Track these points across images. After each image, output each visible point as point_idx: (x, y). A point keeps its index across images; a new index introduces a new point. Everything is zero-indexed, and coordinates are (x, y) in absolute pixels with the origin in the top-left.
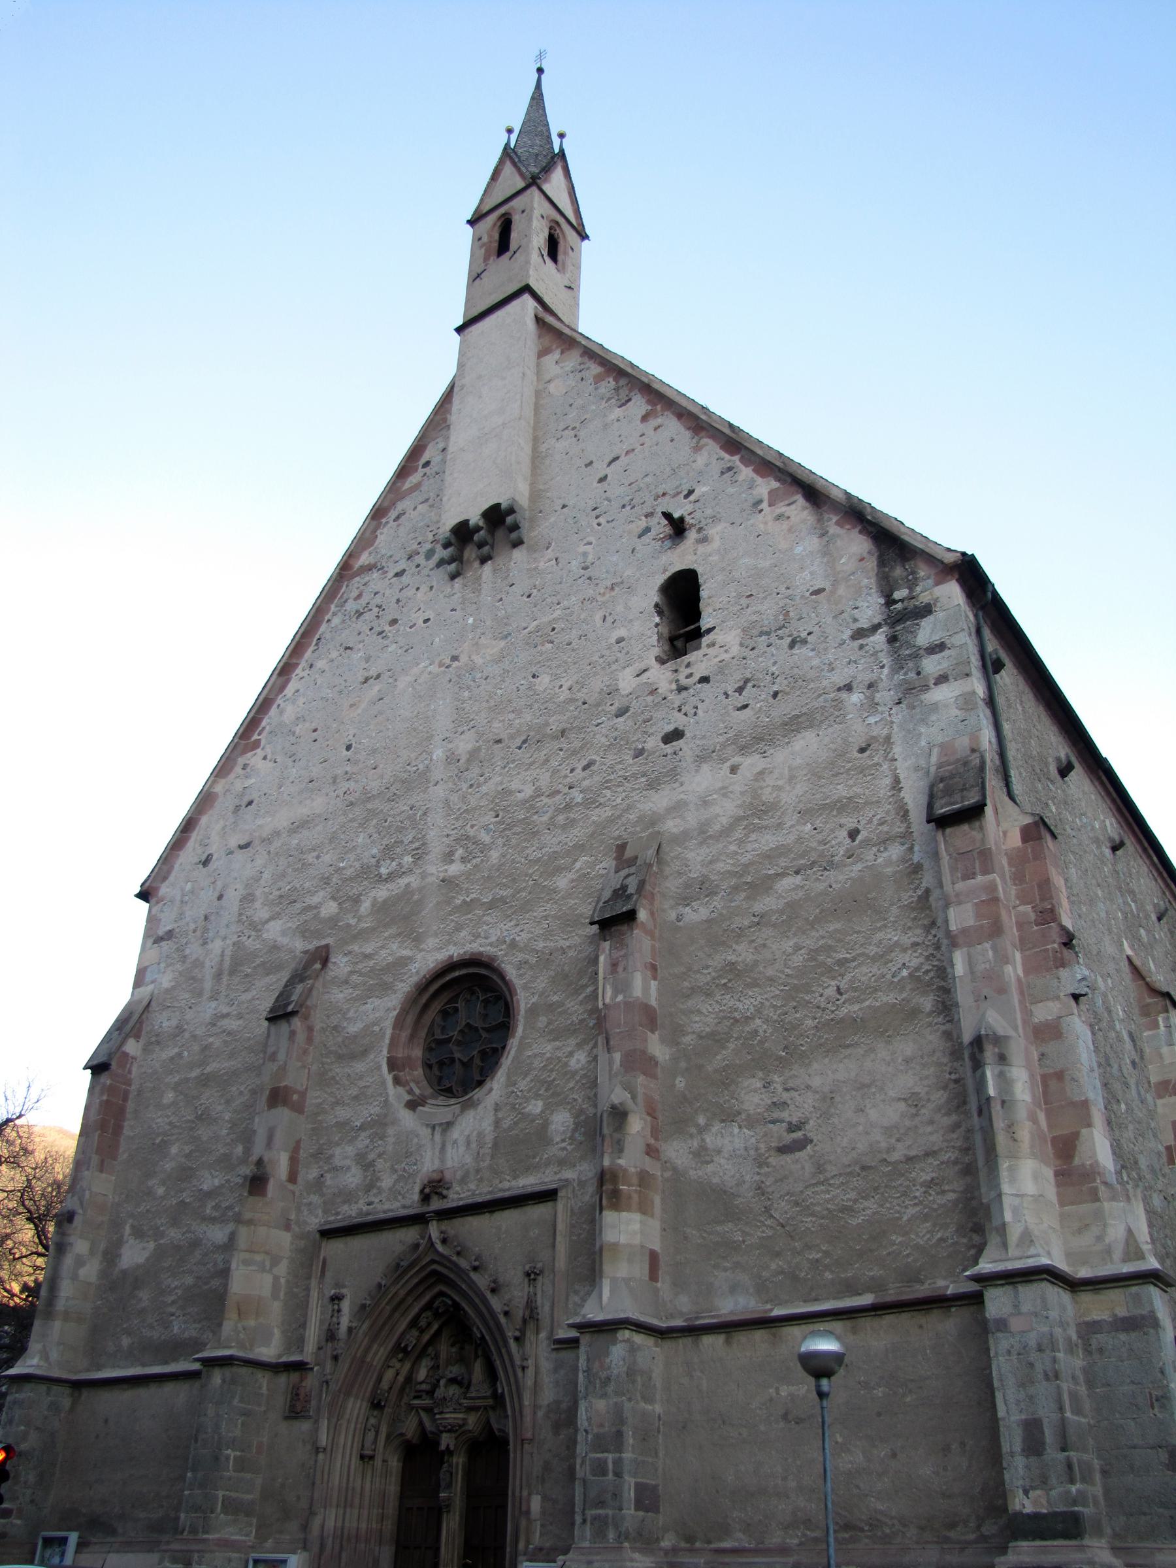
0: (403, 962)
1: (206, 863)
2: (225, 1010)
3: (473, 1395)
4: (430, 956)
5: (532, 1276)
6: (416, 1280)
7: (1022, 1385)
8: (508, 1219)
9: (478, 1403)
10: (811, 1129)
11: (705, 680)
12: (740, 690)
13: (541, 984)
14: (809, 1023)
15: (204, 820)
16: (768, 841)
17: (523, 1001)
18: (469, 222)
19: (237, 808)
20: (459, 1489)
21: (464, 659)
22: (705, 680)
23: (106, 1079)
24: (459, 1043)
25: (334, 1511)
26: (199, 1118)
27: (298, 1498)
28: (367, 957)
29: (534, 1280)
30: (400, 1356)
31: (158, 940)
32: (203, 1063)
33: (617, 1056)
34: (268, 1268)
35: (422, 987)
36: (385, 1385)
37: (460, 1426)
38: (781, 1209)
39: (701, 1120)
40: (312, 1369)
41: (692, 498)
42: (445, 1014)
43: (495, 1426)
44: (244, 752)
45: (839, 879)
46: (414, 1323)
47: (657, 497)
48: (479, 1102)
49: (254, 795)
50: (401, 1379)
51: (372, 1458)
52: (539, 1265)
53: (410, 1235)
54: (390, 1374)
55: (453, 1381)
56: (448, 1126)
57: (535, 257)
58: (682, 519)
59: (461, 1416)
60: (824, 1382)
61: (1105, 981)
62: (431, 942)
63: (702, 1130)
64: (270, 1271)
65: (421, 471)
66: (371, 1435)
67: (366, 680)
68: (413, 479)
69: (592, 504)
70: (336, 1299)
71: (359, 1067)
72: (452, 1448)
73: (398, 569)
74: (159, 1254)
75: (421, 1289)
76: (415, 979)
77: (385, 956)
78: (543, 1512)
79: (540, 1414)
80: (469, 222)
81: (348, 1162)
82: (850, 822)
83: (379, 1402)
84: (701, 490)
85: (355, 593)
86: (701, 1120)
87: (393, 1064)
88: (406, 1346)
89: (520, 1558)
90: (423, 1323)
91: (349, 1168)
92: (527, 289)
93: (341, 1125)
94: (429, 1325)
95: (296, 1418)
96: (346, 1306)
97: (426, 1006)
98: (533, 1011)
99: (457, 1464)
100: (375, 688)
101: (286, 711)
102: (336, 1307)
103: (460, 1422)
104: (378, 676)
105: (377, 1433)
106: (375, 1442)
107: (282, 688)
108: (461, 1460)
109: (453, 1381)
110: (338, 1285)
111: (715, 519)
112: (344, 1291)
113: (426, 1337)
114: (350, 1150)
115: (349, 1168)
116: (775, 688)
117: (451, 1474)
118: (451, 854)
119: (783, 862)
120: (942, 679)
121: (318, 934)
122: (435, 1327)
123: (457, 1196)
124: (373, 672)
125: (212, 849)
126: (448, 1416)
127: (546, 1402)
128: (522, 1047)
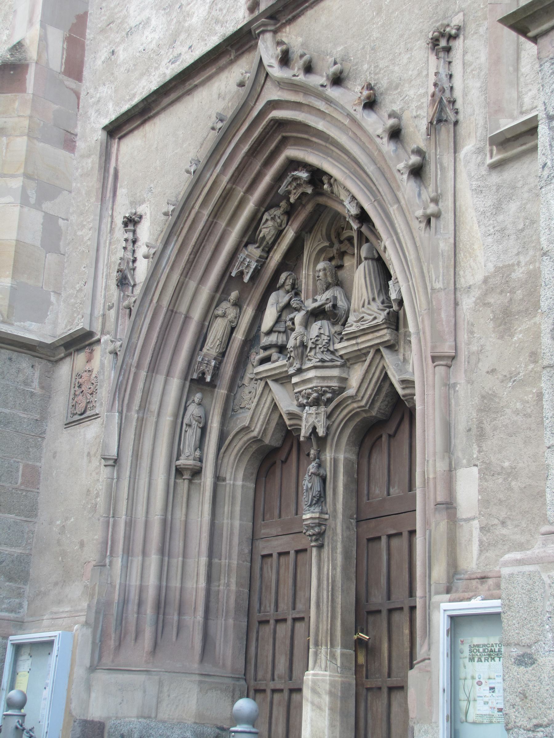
3: (353, 329)
5: (443, 43)
6: (245, 148)
9: (365, 341)
25: (324, 647)
27: (82, 544)
29: (448, 50)
30: (234, 295)
34: (32, 201)
36: (212, 347)
37: (337, 392)
40: (99, 341)
46: (250, 234)
50: (239, 336)
51: (197, 473)
52: (456, 20)
54: (218, 328)
55: (317, 314)
59: (335, 372)
64: (38, 206)
66: (191, 437)
70: (132, 222)
72: (321, 432)
75: (257, 165)
78: (485, 502)
79: (467, 303)
81: (146, 13)
89: (436, 598)
90: (267, 230)
91: (148, 21)
94: (279, 234)
95: (78, 422)
96: (146, 232)
99: (335, 461)
102: (130, 236)
103: (335, 384)
105: (204, 430)
106: (201, 444)
108: (341, 457)
109: (317, 314)
110: (134, 203)
112: (140, 210)
113: (276, 257)
115: (148, 21)
117: (324, 480)
122: (290, 235)
127: (479, 277)
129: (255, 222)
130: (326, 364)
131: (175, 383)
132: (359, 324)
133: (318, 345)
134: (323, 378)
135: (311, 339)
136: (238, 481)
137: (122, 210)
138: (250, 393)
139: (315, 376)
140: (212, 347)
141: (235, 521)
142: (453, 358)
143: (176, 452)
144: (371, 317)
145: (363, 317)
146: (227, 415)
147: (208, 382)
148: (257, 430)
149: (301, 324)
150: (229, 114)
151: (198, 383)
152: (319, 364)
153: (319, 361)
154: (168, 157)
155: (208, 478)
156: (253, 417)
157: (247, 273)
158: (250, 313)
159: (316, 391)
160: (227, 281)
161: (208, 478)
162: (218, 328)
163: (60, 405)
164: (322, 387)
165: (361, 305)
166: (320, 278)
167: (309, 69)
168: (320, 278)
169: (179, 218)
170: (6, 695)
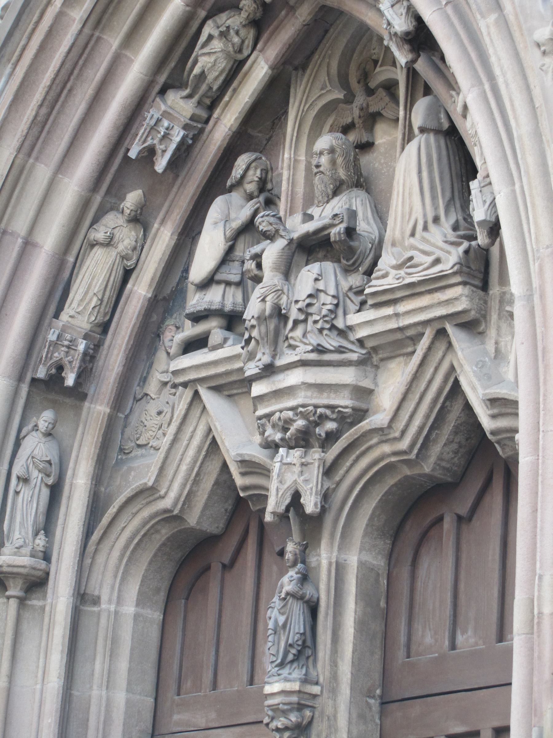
3: (390, 282)
20: (345, 669)
43: (475, 394)
46: (173, 67)
48: (357, 71)
54: (95, 272)
55: (312, 247)
59: (347, 376)
60: (43, 532)
83: (55, 380)
88: (150, 153)
90: (209, 59)
94: (236, 69)
99: (340, 569)
103: (344, 401)
105: (55, 491)
108: (353, 560)
109: (312, 247)
113: (227, 120)
117: (313, 609)
126: (294, 378)
130: (327, 357)
132: (402, 272)
133: (311, 314)
134: (320, 387)
135: (297, 302)
139: (303, 383)
144: (429, 260)
145: (411, 258)
147: (68, 388)
148: (172, 495)
152: (313, 356)
153: (312, 351)
157: (164, 151)
158: (167, 239)
159: (304, 416)
164: (316, 407)
165: (408, 232)
166: (321, 169)
168: (321, 169)
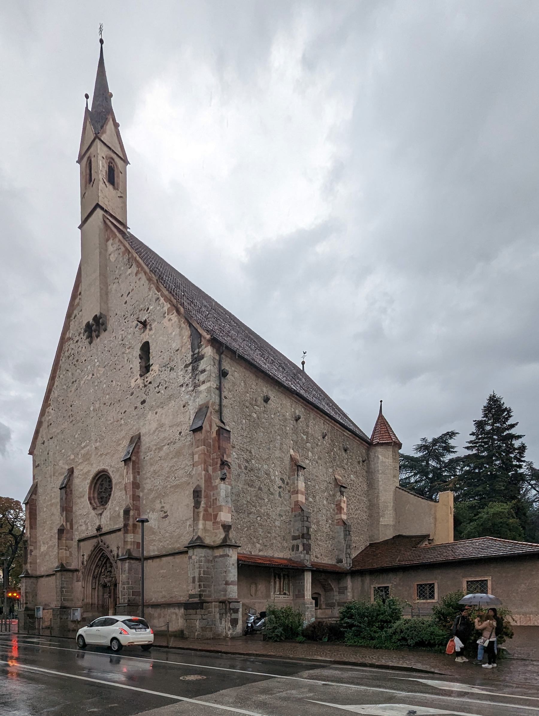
0: (89, 471)
1: (43, 443)
2: (54, 486)
4: (94, 471)
7: (193, 570)
8: (113, 535)
10: (168, 513)
11: (150, 383)
12: (158, 386)
13: (117, 477)
14: (169, 486)
15: (41, 430)
16: (162, 435)
17: (114, 481)
18: (77, 162)
19: (48, 426)
21: (95, 374)
22: (150, 383)
23: (28, 506)
24: (104, 492)
26: (52, 514)
28: (82, 470)
31: (37, 467)
32: (51, 500)
33: (128, 496)
35: (94, 478)
36: (96, 573)
38: (163, 532)
39: (148, 511)
41: (148, 311)
42: (102, 485)
44: (47, 408)
45: (177, 446)
46: (100, 559)
47: (140, 311)
49: (52, 422)
51: (95, 588)
53: (95, 540)
54: (96, 571)
56: (101, 514)
57: (101, 185)
58: (145, 321)
61: (506, 415)
62: (94, 466)
63: (149, 513)
65: (79, 297)
66: (94, 584)
67: (73, 382)
68: (77, 301)
69: (123, 314)
70: (83, 555)
71: (82, 500)
73: (77, 340)
74: (49, 548)
76: (92, 476)
77: (85, 470)
80: (77, 162)
82: (179, 429)
84: (151, 308)
85: (67, 349)
86: (148, 511)
87: (90, 499)
90: (102, 559)
92: (98, 206)
93: (80, 515)
96: (85, 557)
97: (96, 483)
98: (116, 484)
100: (76, 385)
101: (55, 394)
104: (76, 381)
107: (53, 385)
109: (108, 572)
111: (154, 320)
114: (83, 521)
116: (166, 385)
118: (97, 440)
119: (166, 441)
120: (204, 382)
121: (70, 464)
123: (104, 530)
124: (74, 380)
125: (44, 439)
128: (114, 495)
129: (100, 558)
131: (91, 578)
136: (101, 588)
137: (82, 554)
138: (101, 579)
140: (96, 573)
141: (101, 594)
142: (183, 637)
143: (92, 586)
146: (99, 581)
149: (179, 308)
150: (96, 545)
151: (94, 577)
154: (88, 548)
155: (97, 589)
156: (102, 582)
160: (97, 566)
161: (97, 589)
162: (96, 571)
163: (75, 578)
167: (105, 544)
169: (90, 557)
170: (215, 421)
